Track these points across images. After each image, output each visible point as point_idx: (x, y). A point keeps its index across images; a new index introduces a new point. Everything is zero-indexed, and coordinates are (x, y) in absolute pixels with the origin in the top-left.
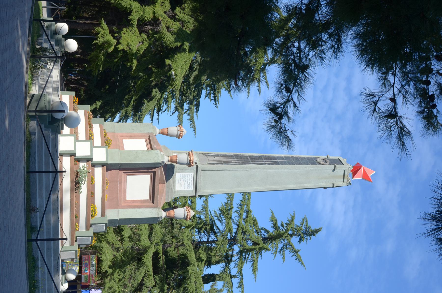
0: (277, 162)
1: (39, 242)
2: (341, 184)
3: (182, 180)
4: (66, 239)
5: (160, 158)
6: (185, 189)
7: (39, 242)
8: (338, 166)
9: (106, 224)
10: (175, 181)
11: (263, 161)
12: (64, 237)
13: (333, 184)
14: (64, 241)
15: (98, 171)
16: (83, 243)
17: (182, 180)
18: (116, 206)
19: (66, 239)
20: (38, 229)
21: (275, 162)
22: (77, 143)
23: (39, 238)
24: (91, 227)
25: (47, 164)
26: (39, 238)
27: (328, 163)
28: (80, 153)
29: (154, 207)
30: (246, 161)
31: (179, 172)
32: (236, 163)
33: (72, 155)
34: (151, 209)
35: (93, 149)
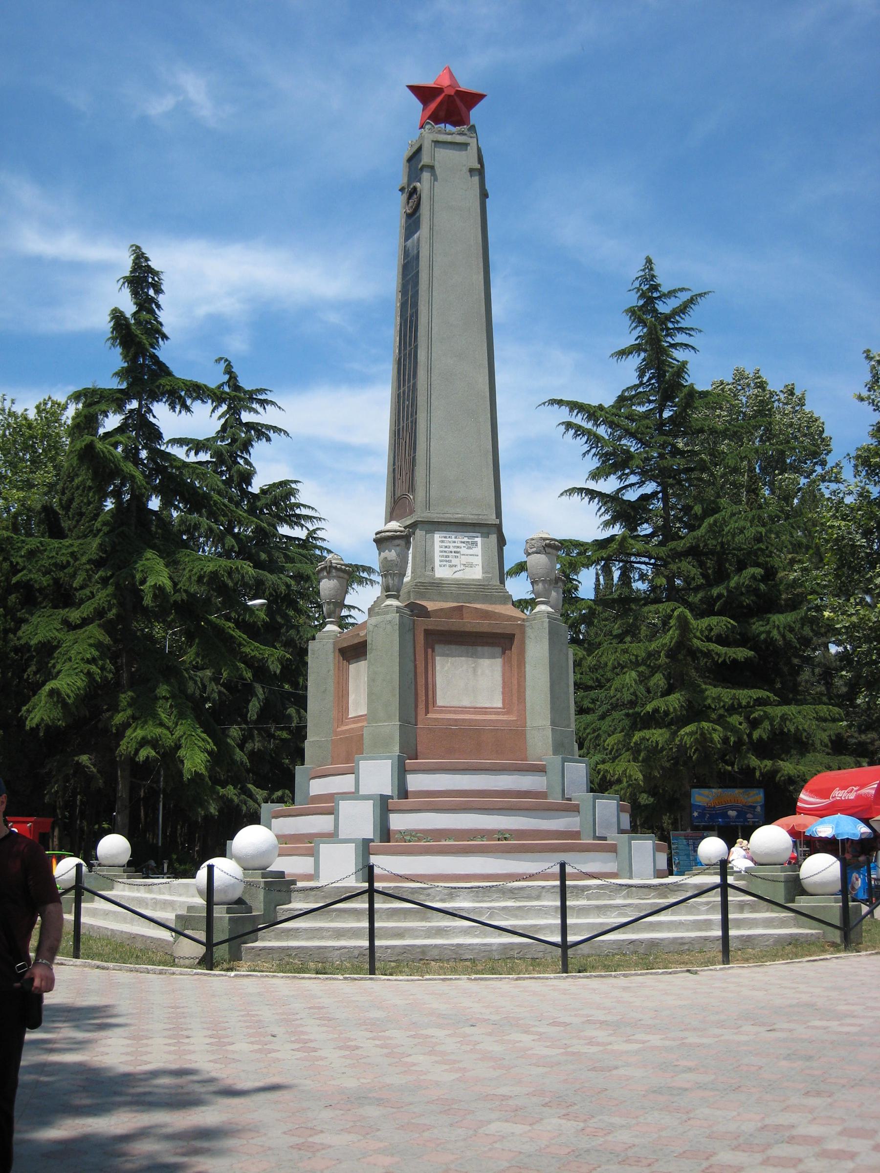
0: (411, 316)
1: (571, 939)
2: (472, 150)
3: (455, 561)
4: (563, 866)
5: (389, 617)
6: (480, 554)
7: (571, 939)
8: (425, 159)
9: (564, 761)
10: (457, 580)
11: (410, 354)
12: (557, 869)
13: (471, 171)
14: (568, 869)
15: (416, 782)
16: (615, 820)
17: (455, 561)
18: (518, 733)
19: (563, 866)
20: (187, 932)
21: (411, 321)
22: (342, 836)
23: (557, 939)
24: (570, 799)
25: (355, 912)
26: (557, 939)
27: (418, 184)
28: (368, 830)
29: (523, 633)
30: (408, 396)
31: (433, 569)
32: (412, 422)
33: (365, 848)
34: (527, 641)
35: (362, 792)
